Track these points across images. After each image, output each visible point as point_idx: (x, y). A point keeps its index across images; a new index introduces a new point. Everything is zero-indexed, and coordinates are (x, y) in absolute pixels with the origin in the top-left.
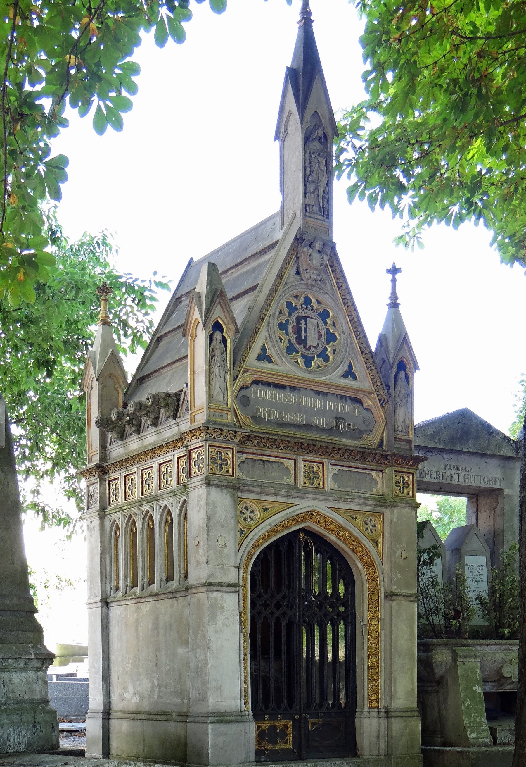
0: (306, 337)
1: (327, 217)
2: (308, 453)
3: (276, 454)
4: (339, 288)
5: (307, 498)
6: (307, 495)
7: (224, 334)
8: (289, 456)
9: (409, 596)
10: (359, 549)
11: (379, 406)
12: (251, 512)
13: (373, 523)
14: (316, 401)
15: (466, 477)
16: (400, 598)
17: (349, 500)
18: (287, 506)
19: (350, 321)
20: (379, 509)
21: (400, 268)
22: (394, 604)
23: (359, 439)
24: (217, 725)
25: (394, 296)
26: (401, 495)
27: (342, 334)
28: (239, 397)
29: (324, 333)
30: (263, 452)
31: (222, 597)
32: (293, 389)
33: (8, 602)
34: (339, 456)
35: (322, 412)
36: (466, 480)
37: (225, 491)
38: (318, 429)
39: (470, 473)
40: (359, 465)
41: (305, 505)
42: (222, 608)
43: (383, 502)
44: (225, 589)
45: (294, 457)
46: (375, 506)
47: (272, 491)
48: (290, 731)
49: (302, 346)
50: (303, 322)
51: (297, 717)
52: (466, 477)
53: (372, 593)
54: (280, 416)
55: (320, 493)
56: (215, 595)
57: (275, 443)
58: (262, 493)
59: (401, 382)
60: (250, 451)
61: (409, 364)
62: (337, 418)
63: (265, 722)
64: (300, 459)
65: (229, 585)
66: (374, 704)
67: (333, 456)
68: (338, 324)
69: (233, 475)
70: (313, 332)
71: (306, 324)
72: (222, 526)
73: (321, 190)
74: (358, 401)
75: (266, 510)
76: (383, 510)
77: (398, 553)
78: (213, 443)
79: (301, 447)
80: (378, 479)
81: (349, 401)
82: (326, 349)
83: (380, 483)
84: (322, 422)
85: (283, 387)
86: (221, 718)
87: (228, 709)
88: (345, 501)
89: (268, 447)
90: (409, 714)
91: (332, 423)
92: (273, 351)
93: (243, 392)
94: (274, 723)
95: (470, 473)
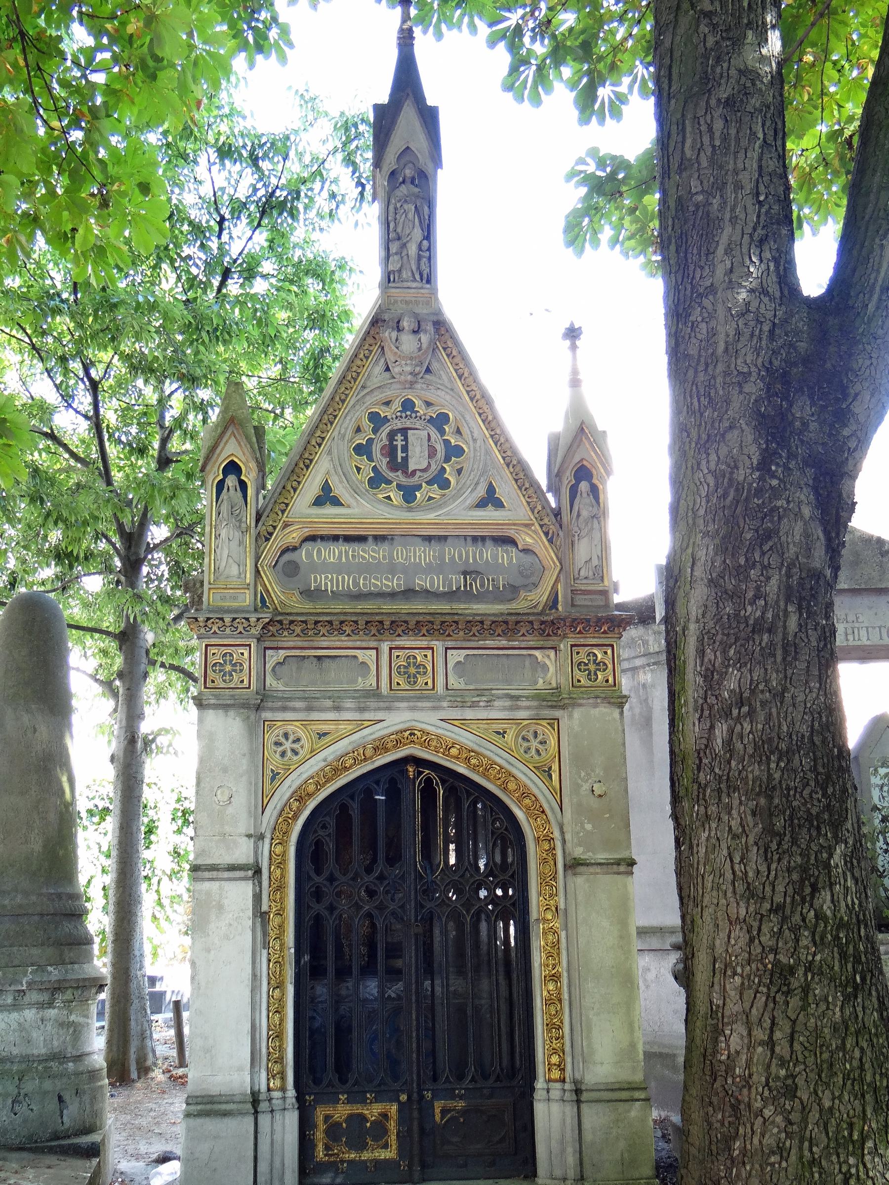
0: (405, 459)
1: (428, 281)
2: (399, 635)
3: (338, 644)
4: (460, 377)
5: (398, 709)
6: (397, 704)
7: (221, 477)
8: (364, 644)
9: (612, 864)
10: (512, 786)
11: (546, 543)
12: (294, 742)
13: (540, 738)
14: (424, 552)
15: (850, 631)
16: (592, 869)
17: (482, 704)
18: (360, 725)
19: (483, 421)
20: (547, 713)
21: (580, 328)
22: (580, 880)
23: (510, 600)
24: (199, 1121)
25: (575, 372)
26: (590, 683)
27: (471, 443)
28: (281, 563)
29: (440, 448)
30: (316, 644)
31: (220, 888)
32: (379, 539)
33: (6, 902)
34: (461, 633)
35: (439, 568)
36: (850, 637)
37: (232, 713)
38: (429, 594)
39: (857, 625)
40: (504, 643)
41: (396, 720)
42: (220, 907)
43: (555, 701)
44: (226, 875)
45: (373, 644)
46: (537, 708)
47: (329, 703)
48: (392, 1126)
49: (399, 473)
50: (399, 437)
51: (404, 1097)
52: (850, 631)
53: (545, 861)
54: (356, 584)
55: (427, 698)
56: (207, 885)
57: (335, 625)
58: (309, 709)
59: (583, 502)
60: (291, 644)
61: (596, 468)
62: (465, 573)
63: (340, 1107)
64: (385, 647)
65: (232, 868)
66: (556, 1074)
67: (449, 635)
68: (465, 430)
69: (249, 688)
70: (418, 449)
71: (406, 439)
72: (225, 770)
73: (413, 249)
74: (509, 541)
75: (322, 735)
76: (558, 713)
77: (586, 787)
78: (213, 641)
79: (380, 627)
80: (548, 662)
81: (489, 543)
82: (443, 470)
83: (552, 670)
84: (438, 584)
85: (361, 539)
86: (209, 1107)
87: (225, 1090)
88: (474, 705)
89: (324, 635)
90: (624, 1095)
91: (456, 581)
92: (341, 488)
93: (287, 557)
94: (357, 1109)
95: (857, 625)
